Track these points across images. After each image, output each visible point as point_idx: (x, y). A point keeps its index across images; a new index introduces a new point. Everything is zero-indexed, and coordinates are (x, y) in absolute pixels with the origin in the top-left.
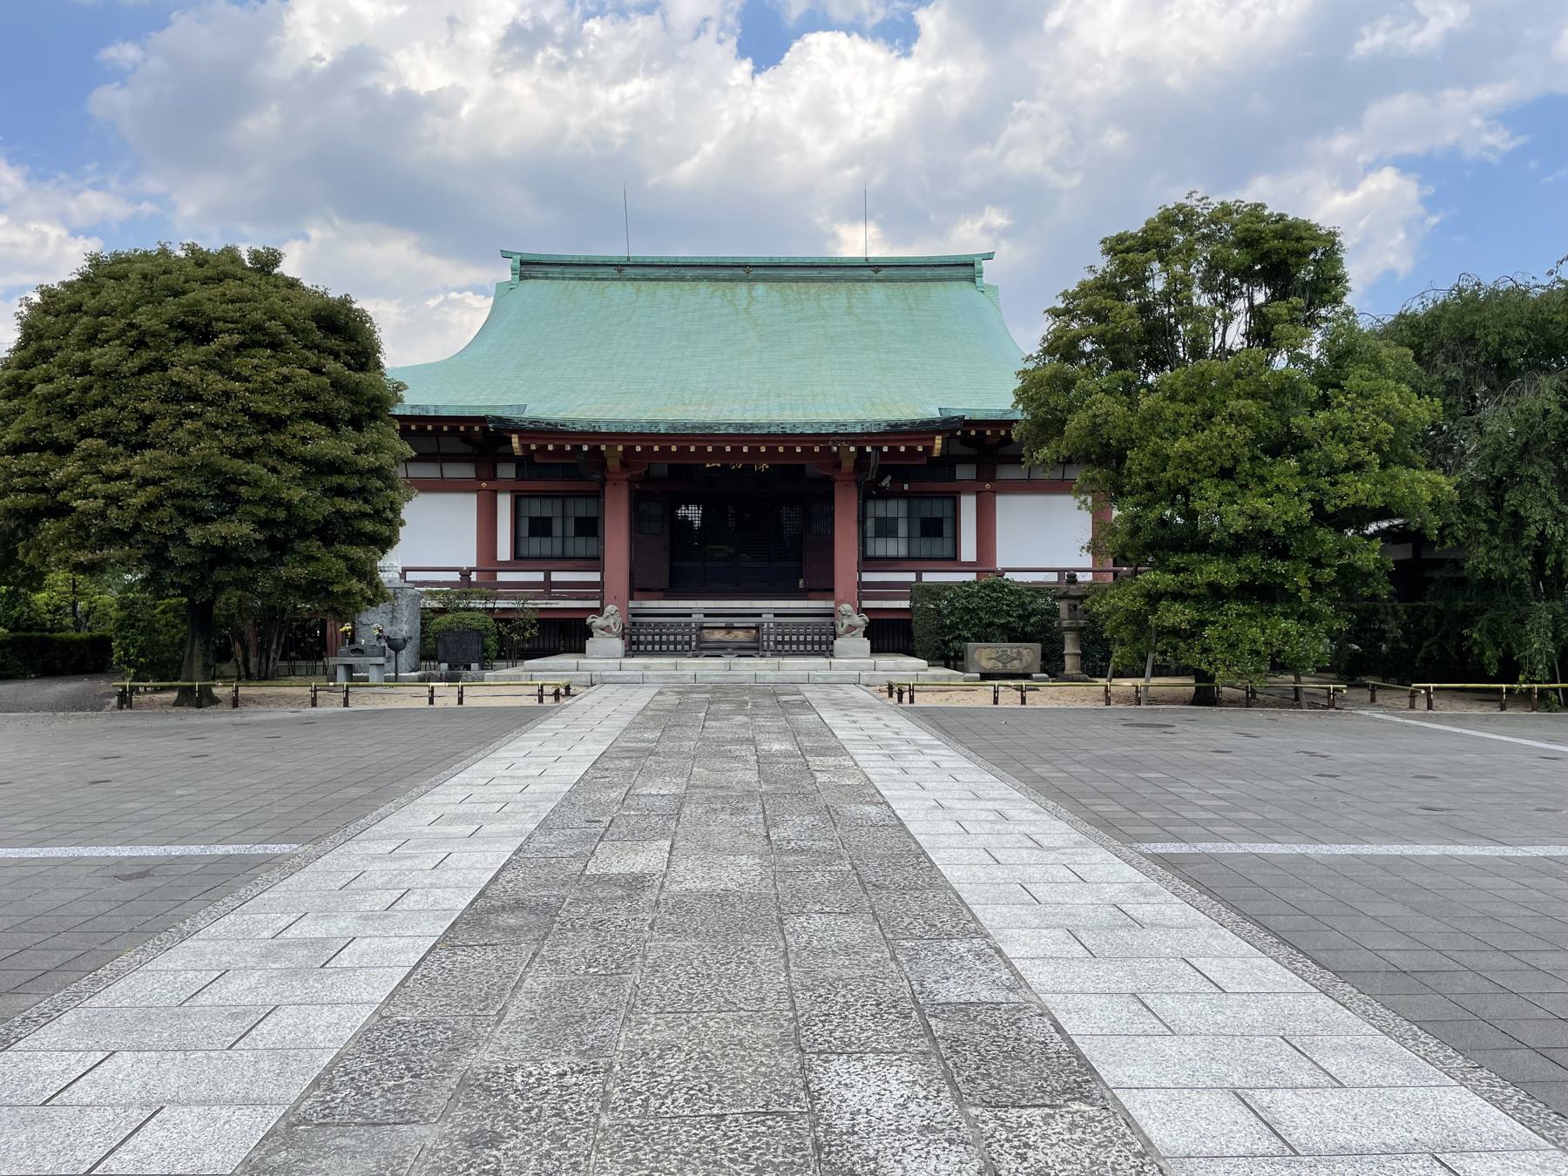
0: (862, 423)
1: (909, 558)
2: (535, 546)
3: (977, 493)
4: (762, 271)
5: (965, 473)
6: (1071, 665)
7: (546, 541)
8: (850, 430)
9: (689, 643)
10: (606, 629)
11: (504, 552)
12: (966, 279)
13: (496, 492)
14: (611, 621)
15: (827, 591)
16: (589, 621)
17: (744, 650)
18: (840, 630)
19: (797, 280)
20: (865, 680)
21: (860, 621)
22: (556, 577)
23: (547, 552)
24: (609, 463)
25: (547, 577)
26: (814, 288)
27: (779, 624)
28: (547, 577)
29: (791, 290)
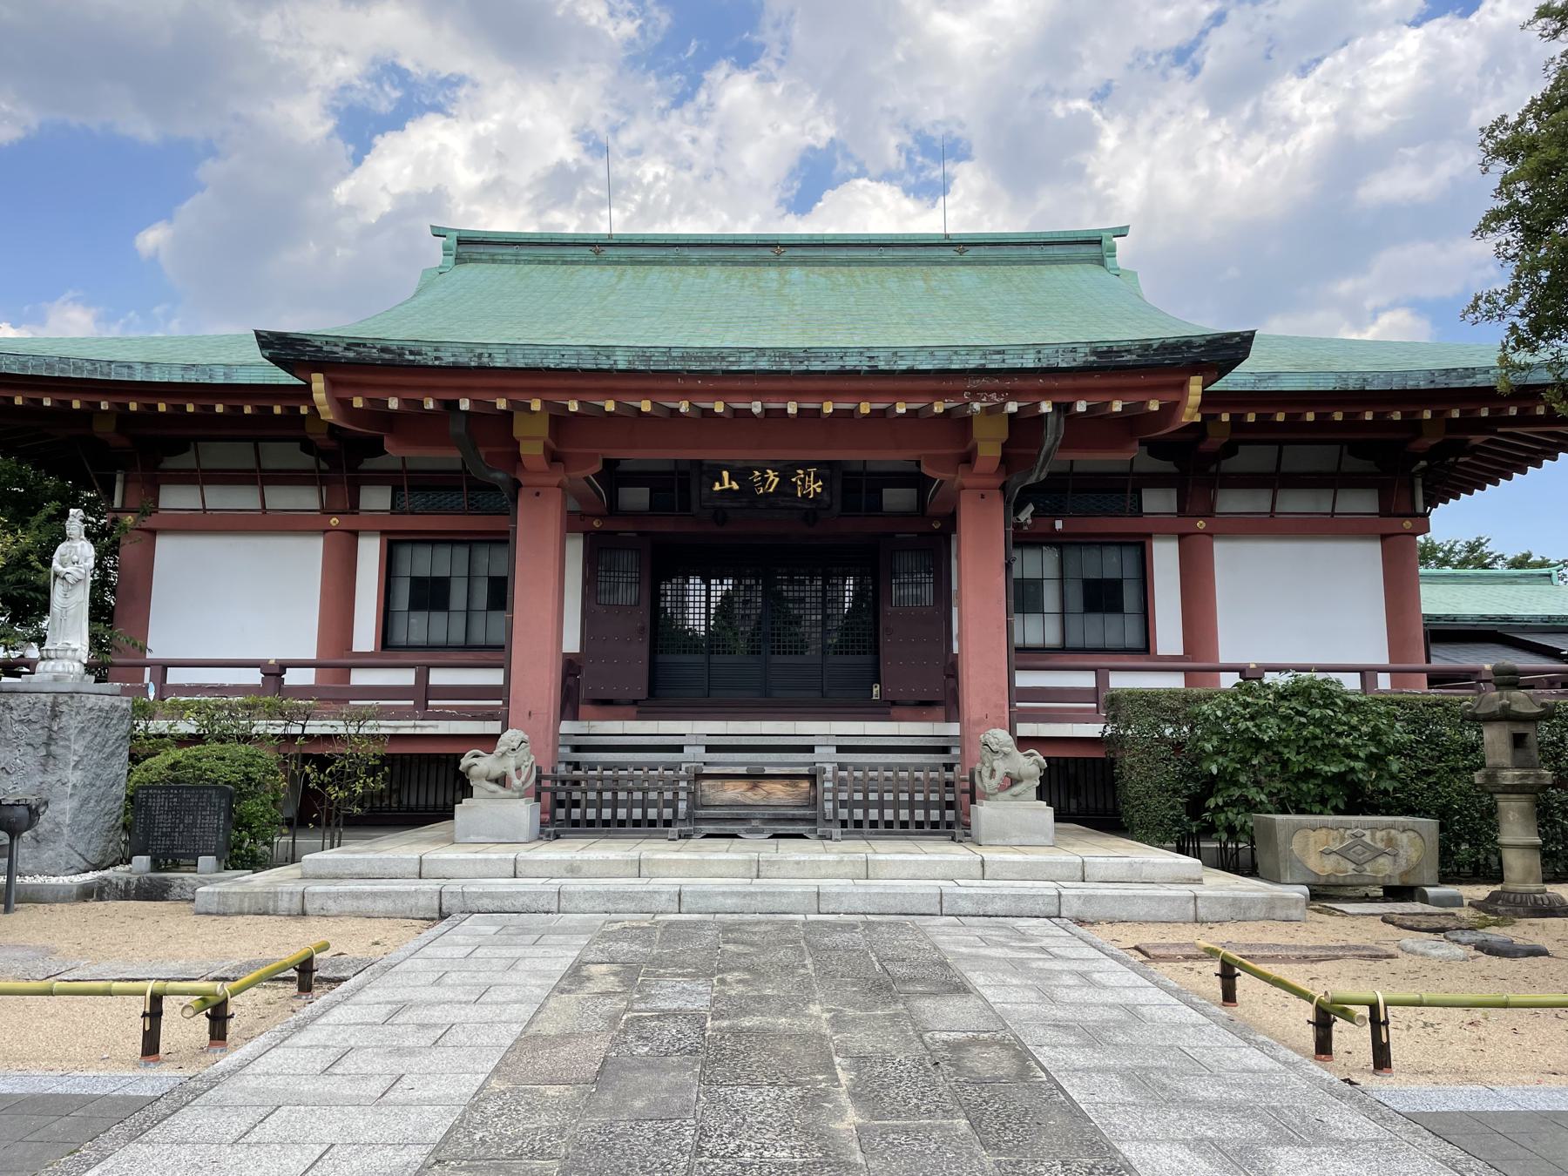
0: (1038, 348)
1: (1063, 649)
2: (416, 627)
3: (1182, 537)
4: (798, 252)
5: (1158, 502)
6: (1520, 868)
7: (439, 618)
8: (1012, 362)
9: (672, 804)
10: (501, 780)
11: (365, 637)
12: (1090, 260)
13: (355, 534)
14: (509, 765)
15: (946, 702)
16: (464, 762)
17: (788, 825)
18: (987, 783)
19: (848, 263)
20: (1072, 908)
21: (1030, 765)
22: (438, 677)
23: (439, 636)
24: (524, 450)
25: (423, 676)
26: (872, 272)
27: (842, 767)
28: (423, 676)
29: (840, 275)
